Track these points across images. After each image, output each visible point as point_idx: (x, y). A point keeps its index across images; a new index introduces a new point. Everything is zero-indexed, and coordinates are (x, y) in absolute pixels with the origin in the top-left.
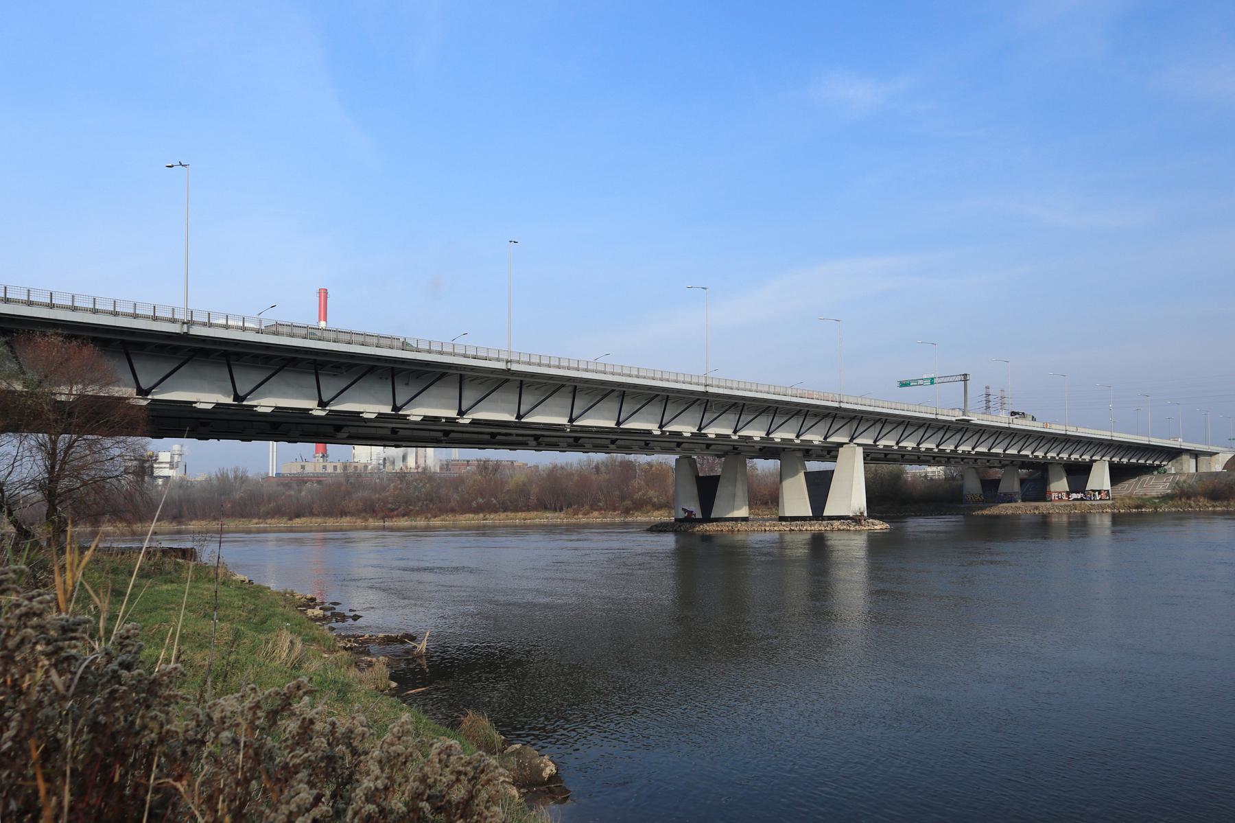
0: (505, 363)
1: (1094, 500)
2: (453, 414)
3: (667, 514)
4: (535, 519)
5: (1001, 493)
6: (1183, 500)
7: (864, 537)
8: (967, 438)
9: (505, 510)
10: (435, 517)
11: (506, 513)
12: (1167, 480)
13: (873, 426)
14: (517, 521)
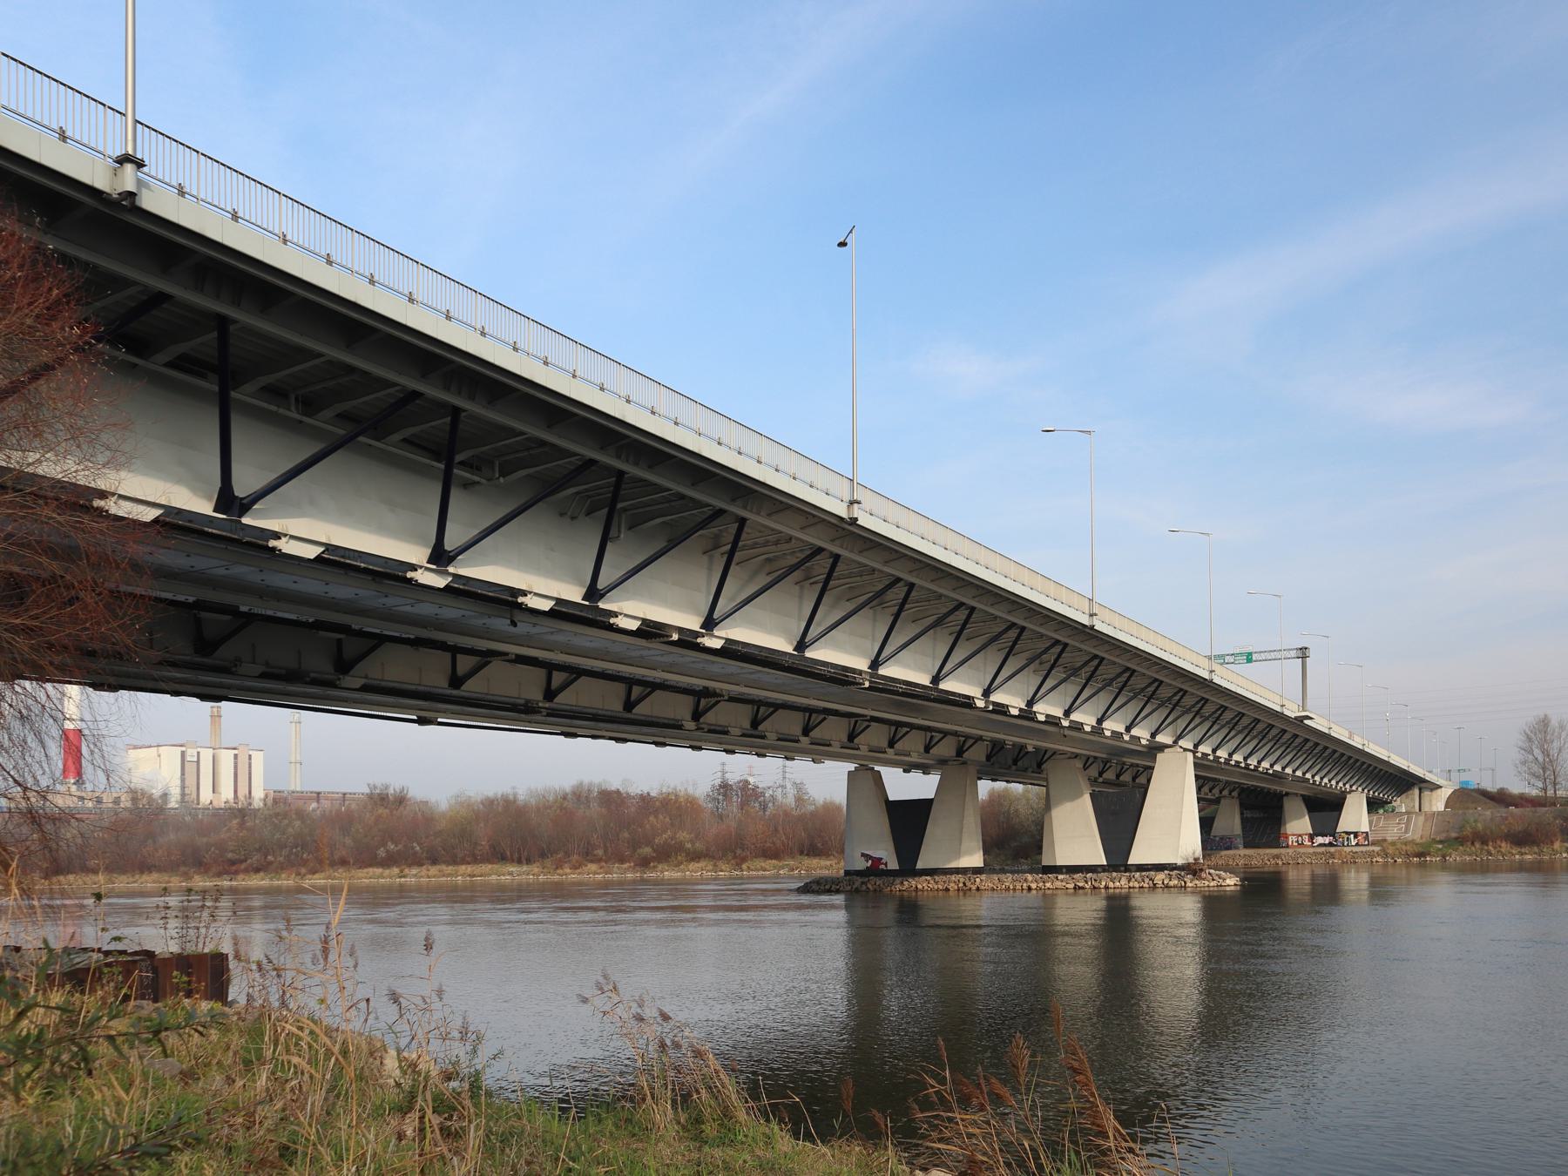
1: (1348, 845)
2: (693, 623)
4: (490, 875)
5: (1215, 836)
6: (1478, 845)
7: (1100, 903)
9: (434, 861)
10: (314, 873)
11: (438, 867)
14: (460, 878)
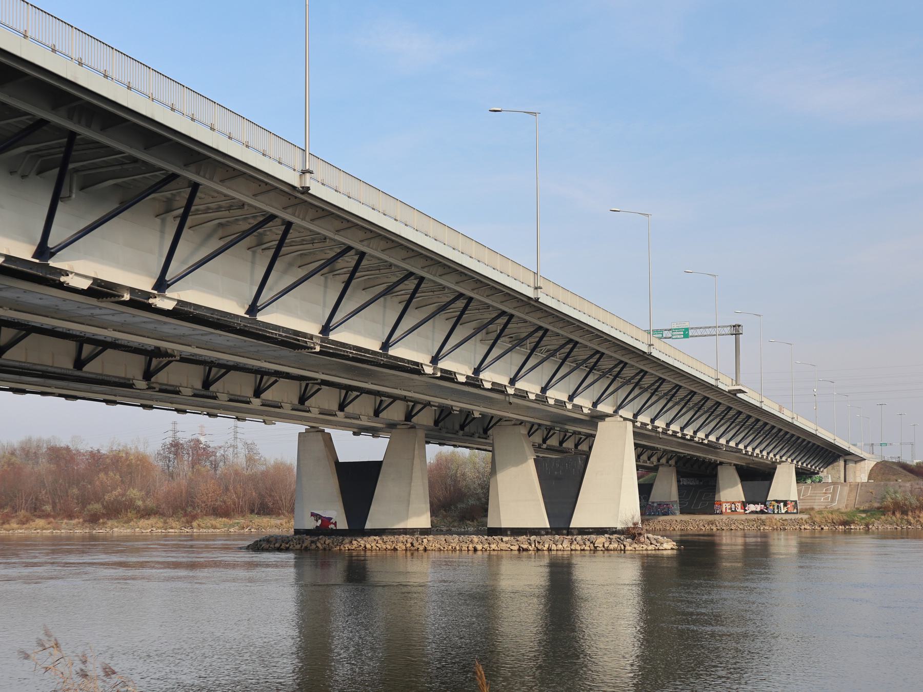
0: (297, 174)
1: (778, 513)
3: (161, 525)
5: (653, 503)
6: (898, 515)
8: (500, 352)
12: (826, 490)
13: (382, 299)
